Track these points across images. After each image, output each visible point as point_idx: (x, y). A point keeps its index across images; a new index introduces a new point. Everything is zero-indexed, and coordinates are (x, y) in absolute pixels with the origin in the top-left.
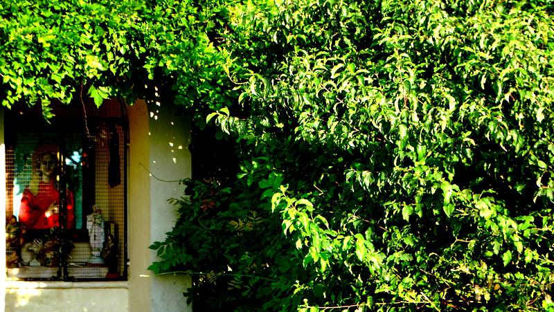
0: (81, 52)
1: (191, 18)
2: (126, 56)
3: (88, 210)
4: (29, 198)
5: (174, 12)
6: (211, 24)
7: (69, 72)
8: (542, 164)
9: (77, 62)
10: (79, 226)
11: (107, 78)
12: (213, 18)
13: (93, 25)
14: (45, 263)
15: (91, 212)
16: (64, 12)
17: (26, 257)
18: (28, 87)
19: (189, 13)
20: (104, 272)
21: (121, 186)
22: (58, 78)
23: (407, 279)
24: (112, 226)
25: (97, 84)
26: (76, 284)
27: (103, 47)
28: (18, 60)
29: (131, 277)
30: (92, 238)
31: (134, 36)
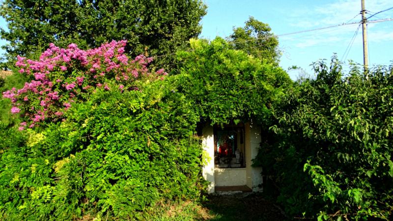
7: (228, 116)
9: (230, 113)
10: (233, 153)
11: (238, 117)
13: (234, 103)
14: (225, 163)
17: (221, 161)
22: (225, 117)
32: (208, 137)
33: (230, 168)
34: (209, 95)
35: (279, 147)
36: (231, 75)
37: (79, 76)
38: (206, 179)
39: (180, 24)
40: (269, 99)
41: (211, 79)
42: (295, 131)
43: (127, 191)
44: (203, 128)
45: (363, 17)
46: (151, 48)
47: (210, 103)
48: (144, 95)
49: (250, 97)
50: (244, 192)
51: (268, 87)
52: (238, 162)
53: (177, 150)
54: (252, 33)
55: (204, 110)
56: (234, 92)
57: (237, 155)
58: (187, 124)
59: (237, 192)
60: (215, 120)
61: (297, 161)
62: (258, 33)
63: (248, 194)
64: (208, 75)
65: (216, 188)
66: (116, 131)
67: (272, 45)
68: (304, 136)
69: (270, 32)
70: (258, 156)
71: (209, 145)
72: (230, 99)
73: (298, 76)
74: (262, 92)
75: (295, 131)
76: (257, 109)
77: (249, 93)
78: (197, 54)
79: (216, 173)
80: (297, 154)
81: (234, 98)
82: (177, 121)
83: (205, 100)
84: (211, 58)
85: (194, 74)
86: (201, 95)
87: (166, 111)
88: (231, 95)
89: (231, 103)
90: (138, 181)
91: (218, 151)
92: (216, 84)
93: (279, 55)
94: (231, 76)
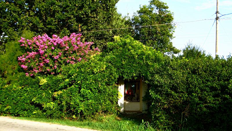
3: (135, 93)
4: (127, 91)
7: (131, 76)
8: (179, 88)
10: (134, 95)
11: (136, 76)
13: (134, 70)
17: (127, 99)
23: (165, 100)
25: (135, 77)
33: (132, 101)
34: (123, 66)
36: (134, 57)
37: (59, 51)
38: (120, 106)
39: (102, 8)
41: (124, 58)
43: (89, 104)
44: (120, 81)
45: (217, 16)
46: (82, 26)
47: (124, 70)
48: (99, 67)
49: (142, 67)
50: (138, 113)
53: (109, 89)
54: (154, 10)
55: (121, 72)
56: (135, 65)
58: (113, 79)
59: (134, 113)
60: (125, 77)
62: (158, 9)
63: (140, 114)
64: (123, 56)
65: (124, 111)
66: (87, 80)
67: (168, 20)
69: (168, 10)
71: (121, 90)
73: (186, 45)
76: (144, 73)
77: (141, 65)
78: (118, 45)
82: (110, 77)
83: (121, 68)
84: (125, 48)
85: (116, 56)
86: (120, 66)
87: (107, 73)
88: (133, 66)
90: (93, 101)
91: (126, 93)
92: (127, 61)
93: (174, 27)
94: (133, 57)
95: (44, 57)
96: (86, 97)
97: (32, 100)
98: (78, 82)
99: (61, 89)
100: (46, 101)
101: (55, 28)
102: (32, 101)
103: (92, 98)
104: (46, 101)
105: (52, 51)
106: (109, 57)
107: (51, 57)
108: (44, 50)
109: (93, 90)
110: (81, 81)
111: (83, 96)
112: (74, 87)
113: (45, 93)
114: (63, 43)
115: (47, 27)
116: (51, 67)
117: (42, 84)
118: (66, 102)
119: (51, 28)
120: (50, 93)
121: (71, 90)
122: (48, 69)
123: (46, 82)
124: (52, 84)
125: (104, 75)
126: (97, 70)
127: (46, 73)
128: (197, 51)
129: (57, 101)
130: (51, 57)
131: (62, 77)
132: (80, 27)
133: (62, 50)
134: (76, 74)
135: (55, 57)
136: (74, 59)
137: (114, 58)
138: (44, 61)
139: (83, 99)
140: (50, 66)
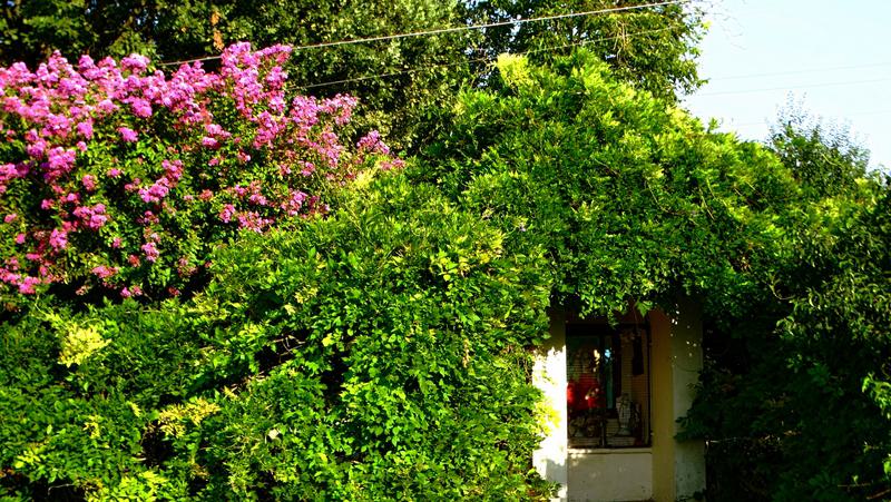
0: (638, 276)
1: (717, 249)
2: (667, 279)
5: (704, 244)
6: (733, 253)
9: (634, 283)
10: (610, 406)
11: (652, 295)
12: (734, 249)
14: (586, 435)
15: (619, 396)
16: (625, 247)
18: (598, 303)
19: (716, 245)
20: (632, 440)
21: (643, 377)
22: (620, 296)
24: (637, 406)
26: (614, 451)
27: (653, 272)
28: (591, 283)
29: (655, 442)
30: (621, 415)
31: (676, 264)
32: (551, 352)
33: (607, 447)
35: (789, 366)
37: (172, 160)
38: (543, 476)
40: (742, 246)
42: (828, 328)
46: (230, 17)
49: (688, 239)
51: (740, 214)
52: (625, 433)
56: (649, 225)
57: (624, 411)
60: (591, 301)
61: (834, 394)
66: (387, 326)
68: (855, 337)
70: (692, 408)
71: (552, 372)
72: (637, 244)
73: (774, 120)
74: (722, 224)
75: (828, 328)
79: (569, 460)
80: (833, 380)
81: (649, 242)
85: (537, 175)
88: (643, 234)
89: (640, 256)
90: (424, 458)
94: (640, 180)
95: (71, 191)
96: (378, 432)
97: (11, 460)
98: (327, 342)
99: (210, 384)
100: (109, 466)
101: (73, 27)
102: (19, 465)
103: (416, 436)
104: (109, 466)
105: (122, 150)
106: (489, 180)
107: (117, 192)
108: (72, 149)
109: (426, 386)
110: (345, 334)
111: (355, 429)
112: (293, 373)
113: (100, 418)
114: (191, 102)
115: (28, 28)
116: (115, 255)
117: (78, 359)
118: (254, 466)
119: (53, 29)
120: (137, 413)
121: (277, 395)
122: (96, 264)
123: (102, 345)
124: (146, 354)
125: (495, 290)
126: (455, 258)
127: (83, 290)
128: (834, 152)
129: (182, 464)
130: (117, 192)
131: (209, 314)
132: (218, 25)
133: (179, 149)
134: (314, 291)
135: (145, 191)
136: (263, 201)
137: (519, 184)
138: (72, 218)
139: (353, 445)
140: (105, 248)
